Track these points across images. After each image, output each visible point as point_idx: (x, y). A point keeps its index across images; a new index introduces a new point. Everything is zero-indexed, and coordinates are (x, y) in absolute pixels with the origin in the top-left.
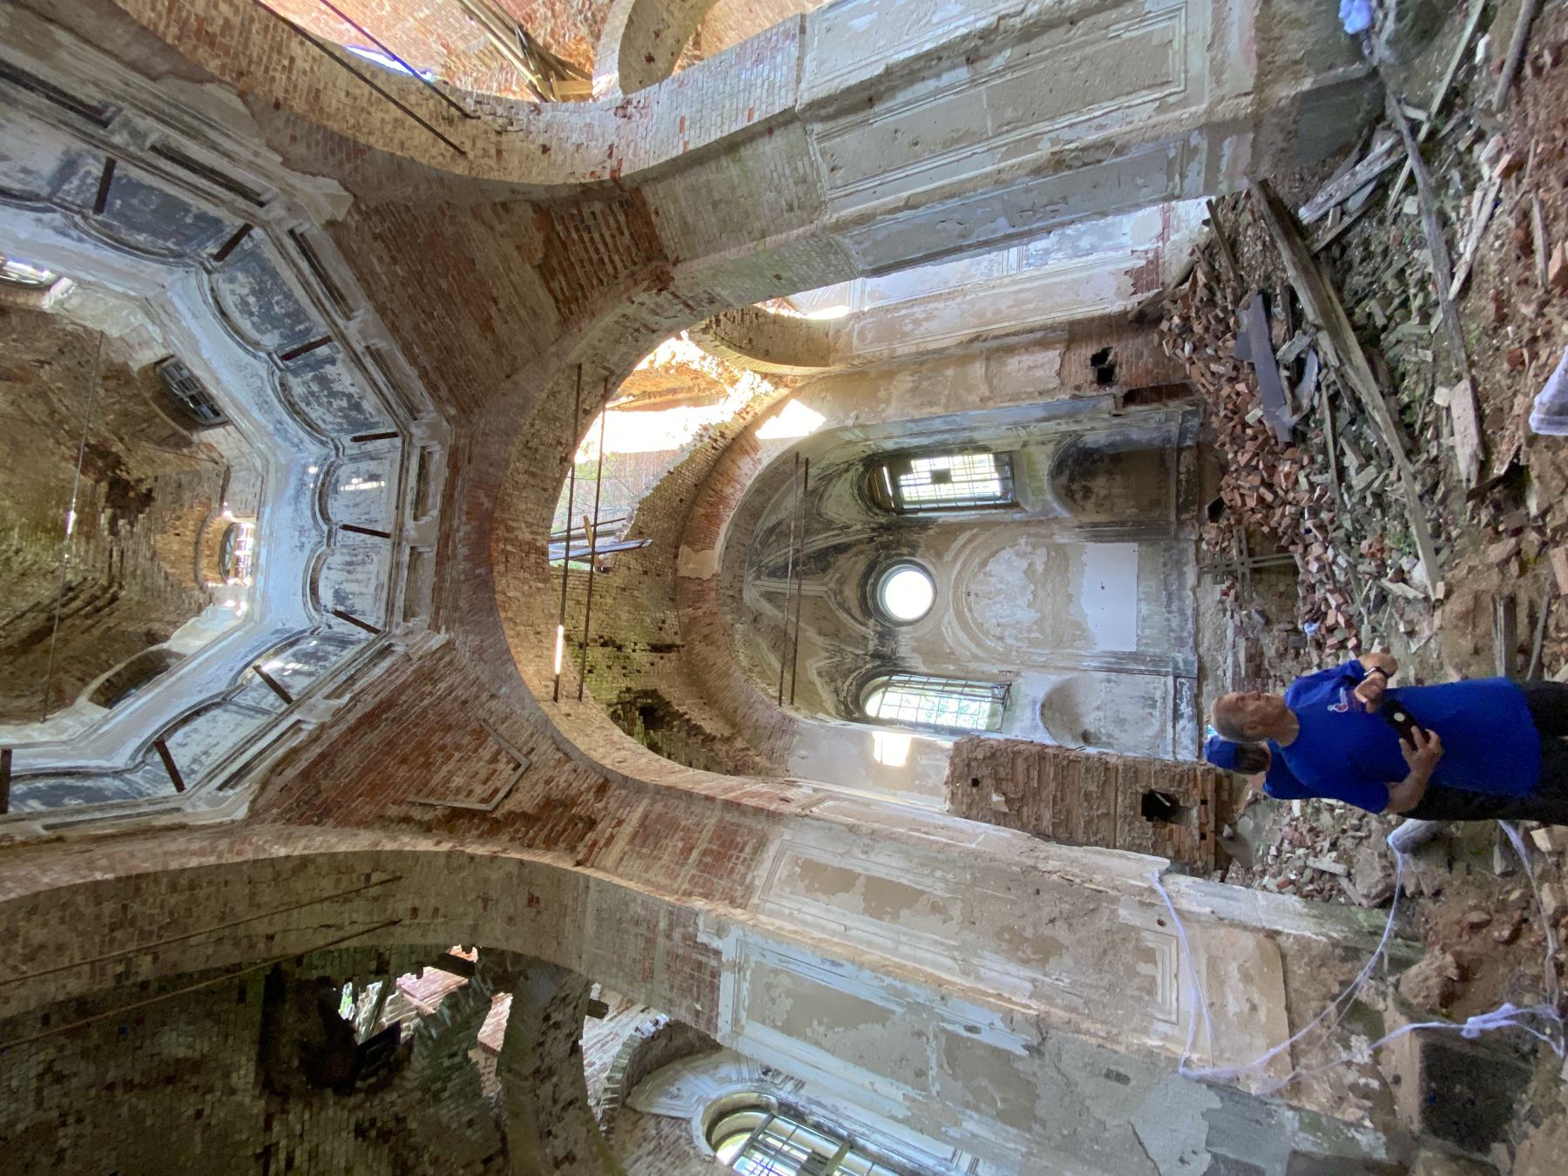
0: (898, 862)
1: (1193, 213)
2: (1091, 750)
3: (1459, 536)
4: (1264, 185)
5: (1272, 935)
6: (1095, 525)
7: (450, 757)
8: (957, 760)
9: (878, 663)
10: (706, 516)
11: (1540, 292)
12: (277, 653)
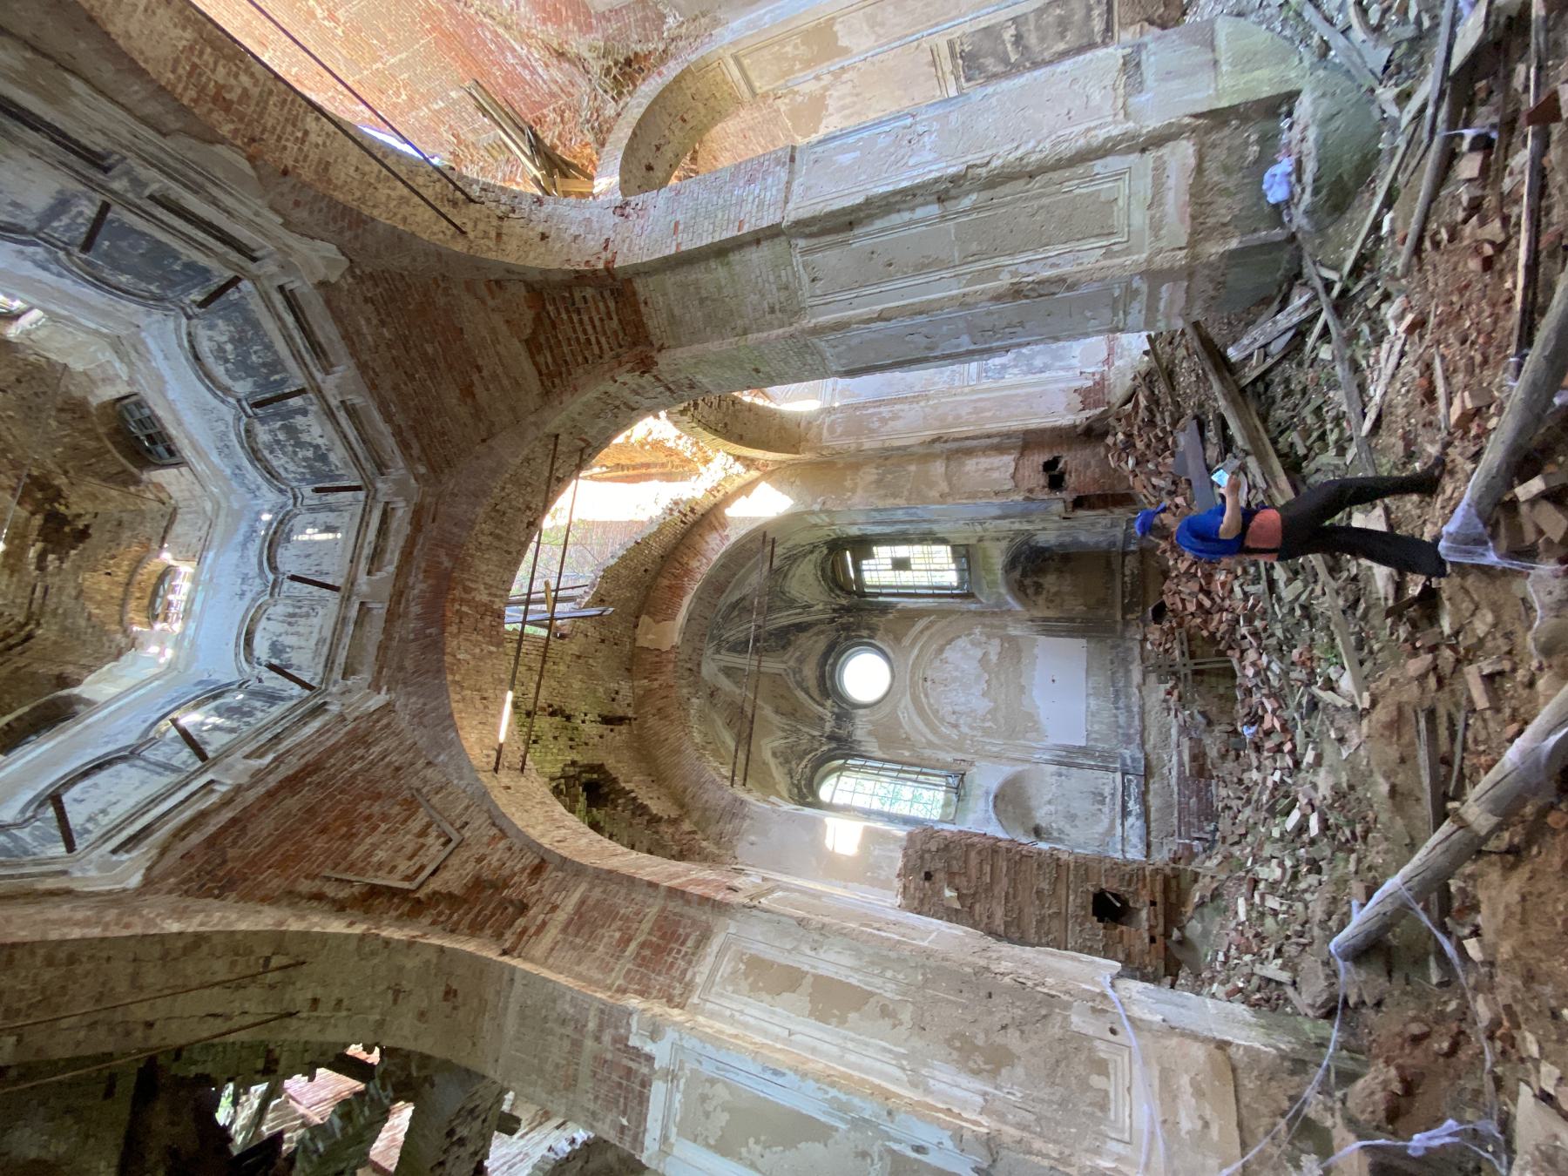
0: (847, 960)
1: (1134, 346)
3: (1380, 650)
5: (1223, 1045)
6: (1045, 619)
9: (834, 745)
11: (1444, 433)
12: (197, 707)
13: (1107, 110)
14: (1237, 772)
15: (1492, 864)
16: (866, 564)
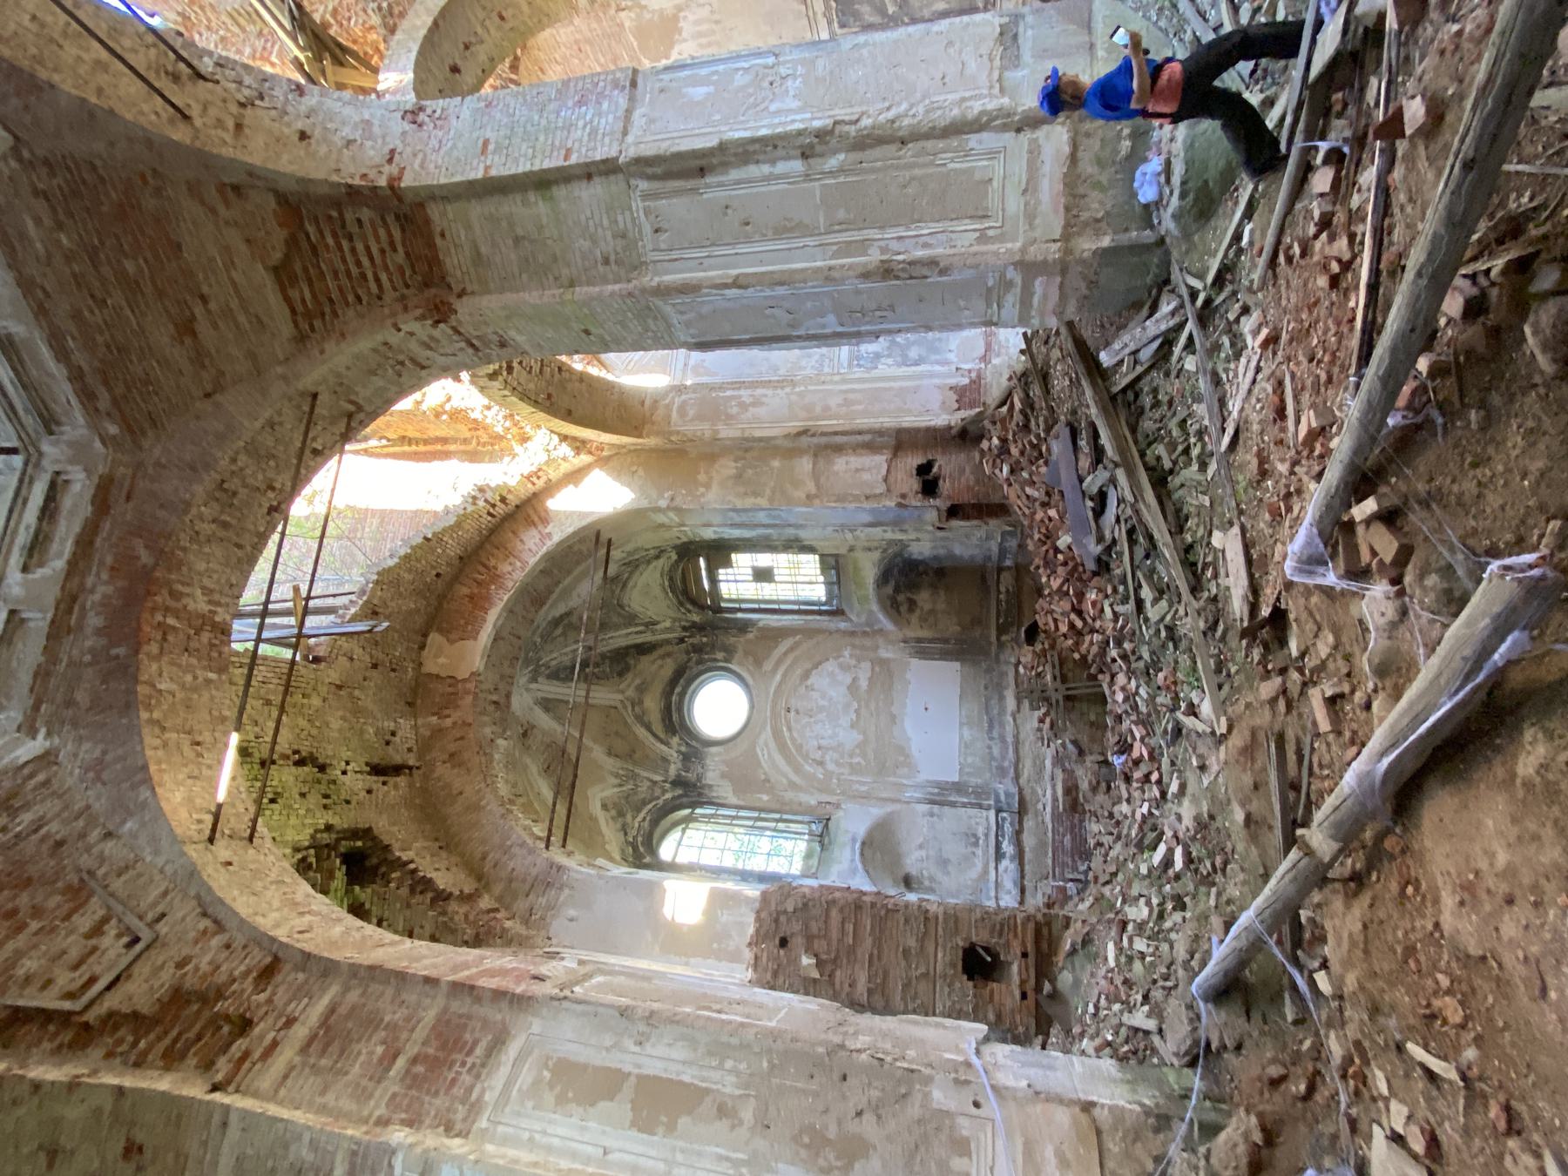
0: (680, 1052)
1: (1011, 340)
2: (912, 897)
3: (1237, 672)
4: (1070, 325)
5: (1088, 1107)
6: (919, 640)
8: (763, 915)
9: (679, 792)
10: (471, 597)
11: (1293, 452)
13: (983, 79)
14: (1108, 804)
15: (1335, 891)
16: (722, 573)
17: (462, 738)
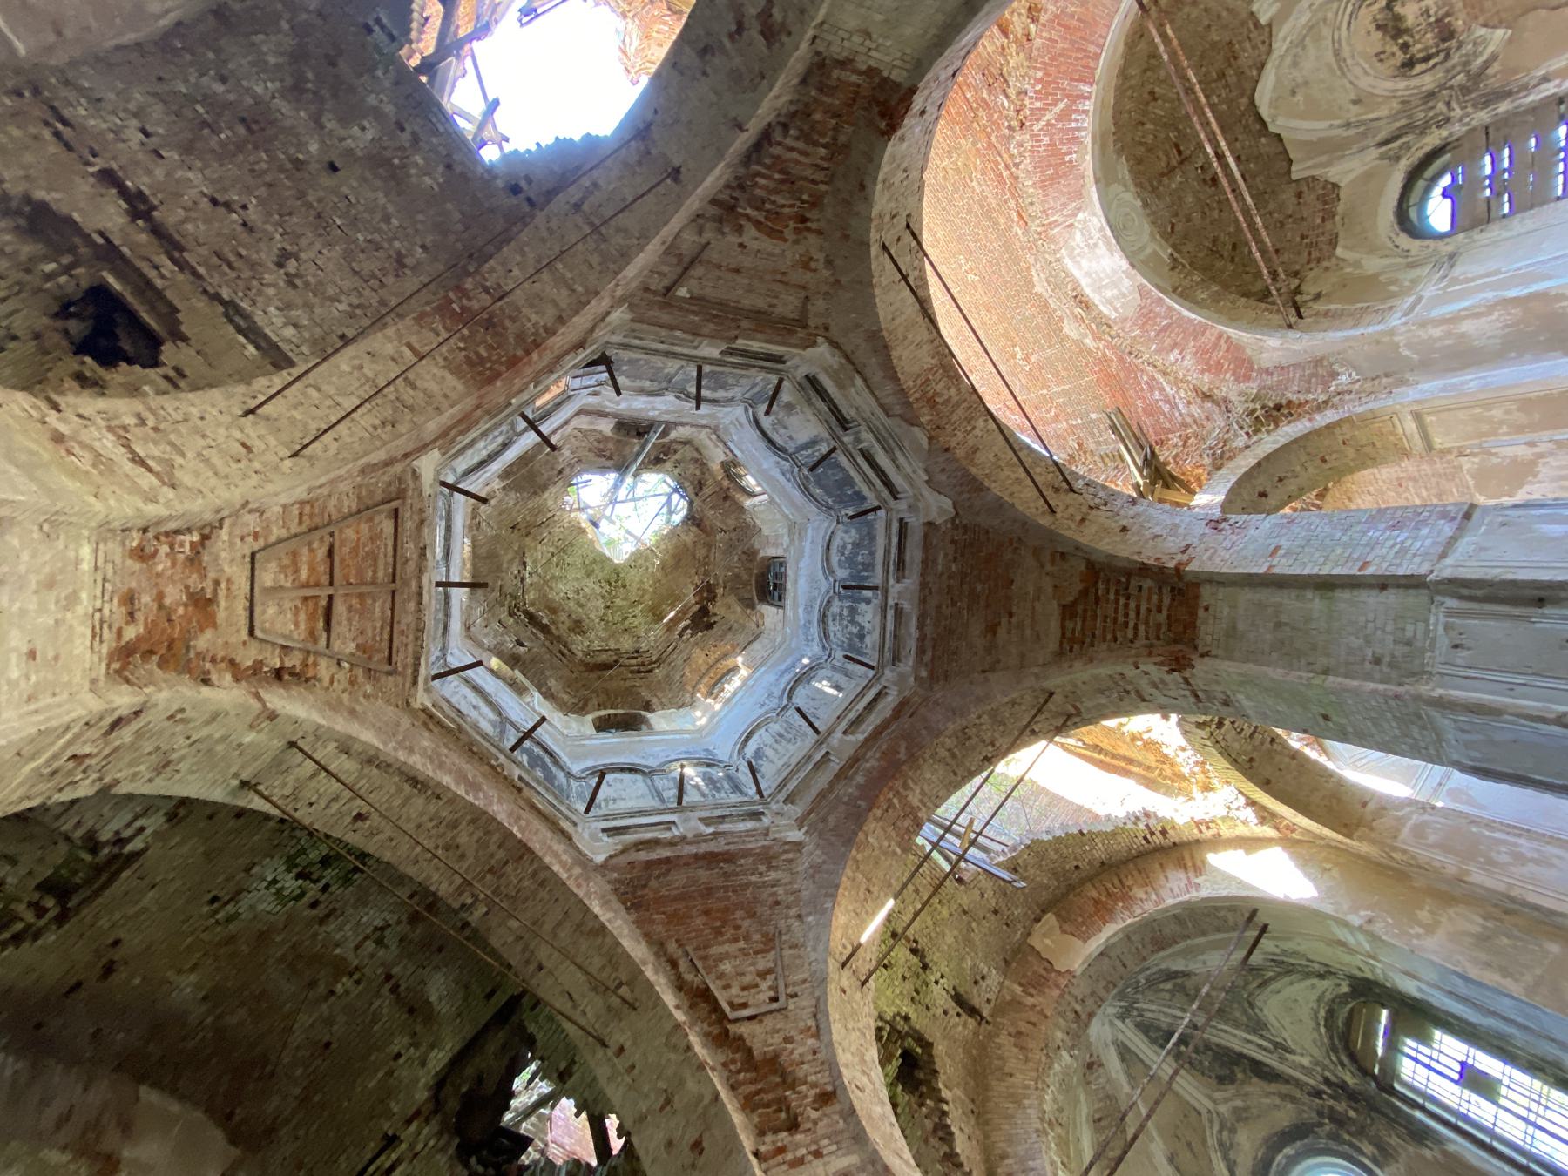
7: (736, 940)
10: (1097, 902)
12: (697, 765)
17: (1034, 1024)
